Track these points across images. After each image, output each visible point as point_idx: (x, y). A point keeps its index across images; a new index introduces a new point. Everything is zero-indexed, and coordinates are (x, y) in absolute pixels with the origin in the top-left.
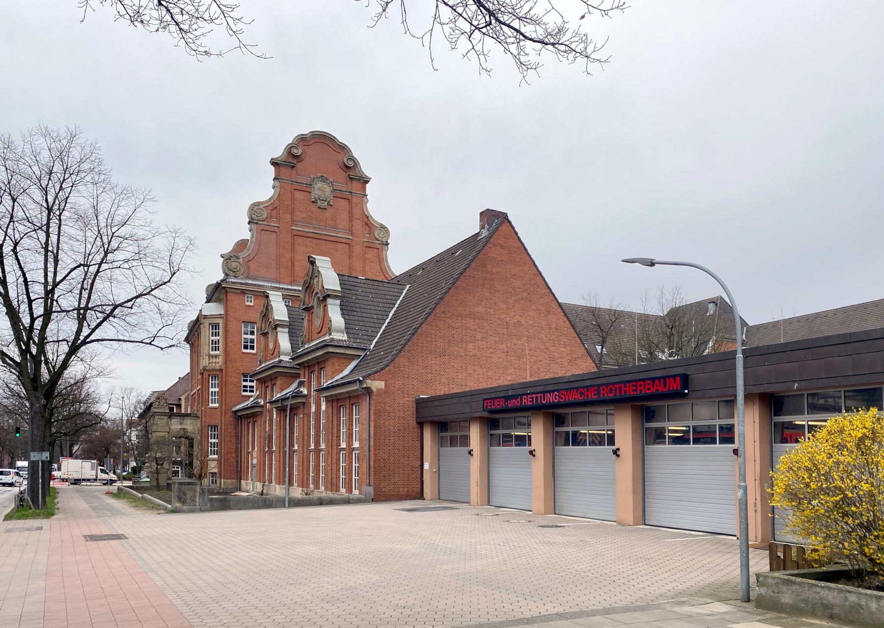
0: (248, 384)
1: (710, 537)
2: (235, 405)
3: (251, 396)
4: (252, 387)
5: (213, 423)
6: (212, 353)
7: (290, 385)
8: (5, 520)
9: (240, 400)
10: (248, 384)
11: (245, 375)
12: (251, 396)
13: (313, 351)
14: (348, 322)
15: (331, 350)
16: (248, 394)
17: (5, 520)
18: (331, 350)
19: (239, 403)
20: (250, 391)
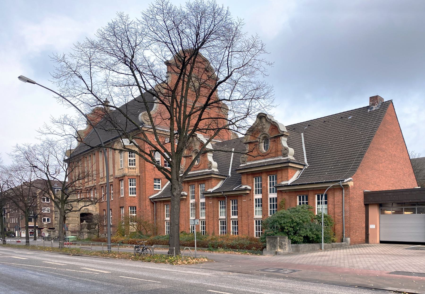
0: (157, 184)
1: (381, 285)
2: (151, 195)
3: (159, 191)
4: (159, 186)
5: (133, 205)
6: (129, 166)
7: (217, 184)
8: (19, 77)
9: (153, 193)
10: (157, 184)
11: (155, 179)
12: (159, 191)
13: (265, 166)
14: (302, 155)
15: (213, 176)
16: (157, 189)
17: (19, 77)
18: (213, 176)
19: (153, 195)
20: (158, 188)
